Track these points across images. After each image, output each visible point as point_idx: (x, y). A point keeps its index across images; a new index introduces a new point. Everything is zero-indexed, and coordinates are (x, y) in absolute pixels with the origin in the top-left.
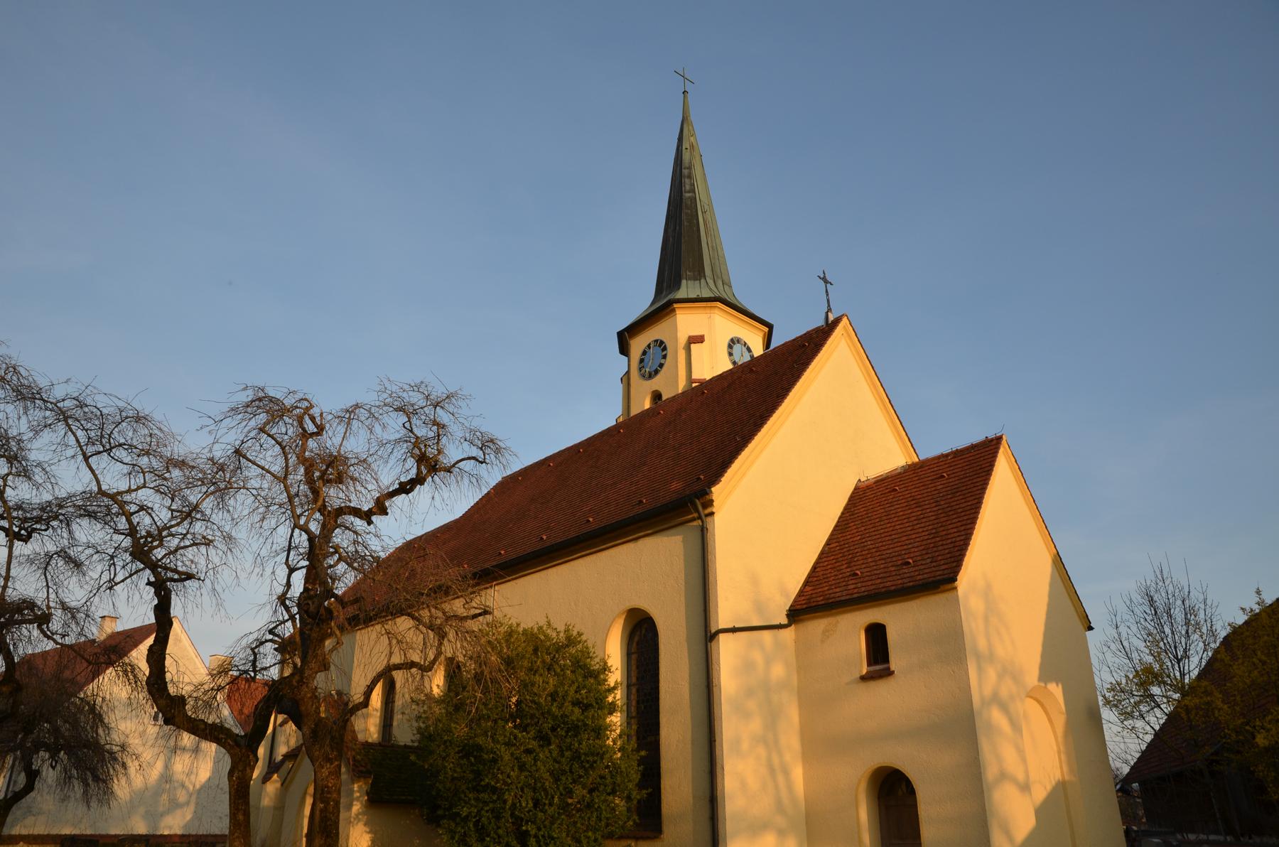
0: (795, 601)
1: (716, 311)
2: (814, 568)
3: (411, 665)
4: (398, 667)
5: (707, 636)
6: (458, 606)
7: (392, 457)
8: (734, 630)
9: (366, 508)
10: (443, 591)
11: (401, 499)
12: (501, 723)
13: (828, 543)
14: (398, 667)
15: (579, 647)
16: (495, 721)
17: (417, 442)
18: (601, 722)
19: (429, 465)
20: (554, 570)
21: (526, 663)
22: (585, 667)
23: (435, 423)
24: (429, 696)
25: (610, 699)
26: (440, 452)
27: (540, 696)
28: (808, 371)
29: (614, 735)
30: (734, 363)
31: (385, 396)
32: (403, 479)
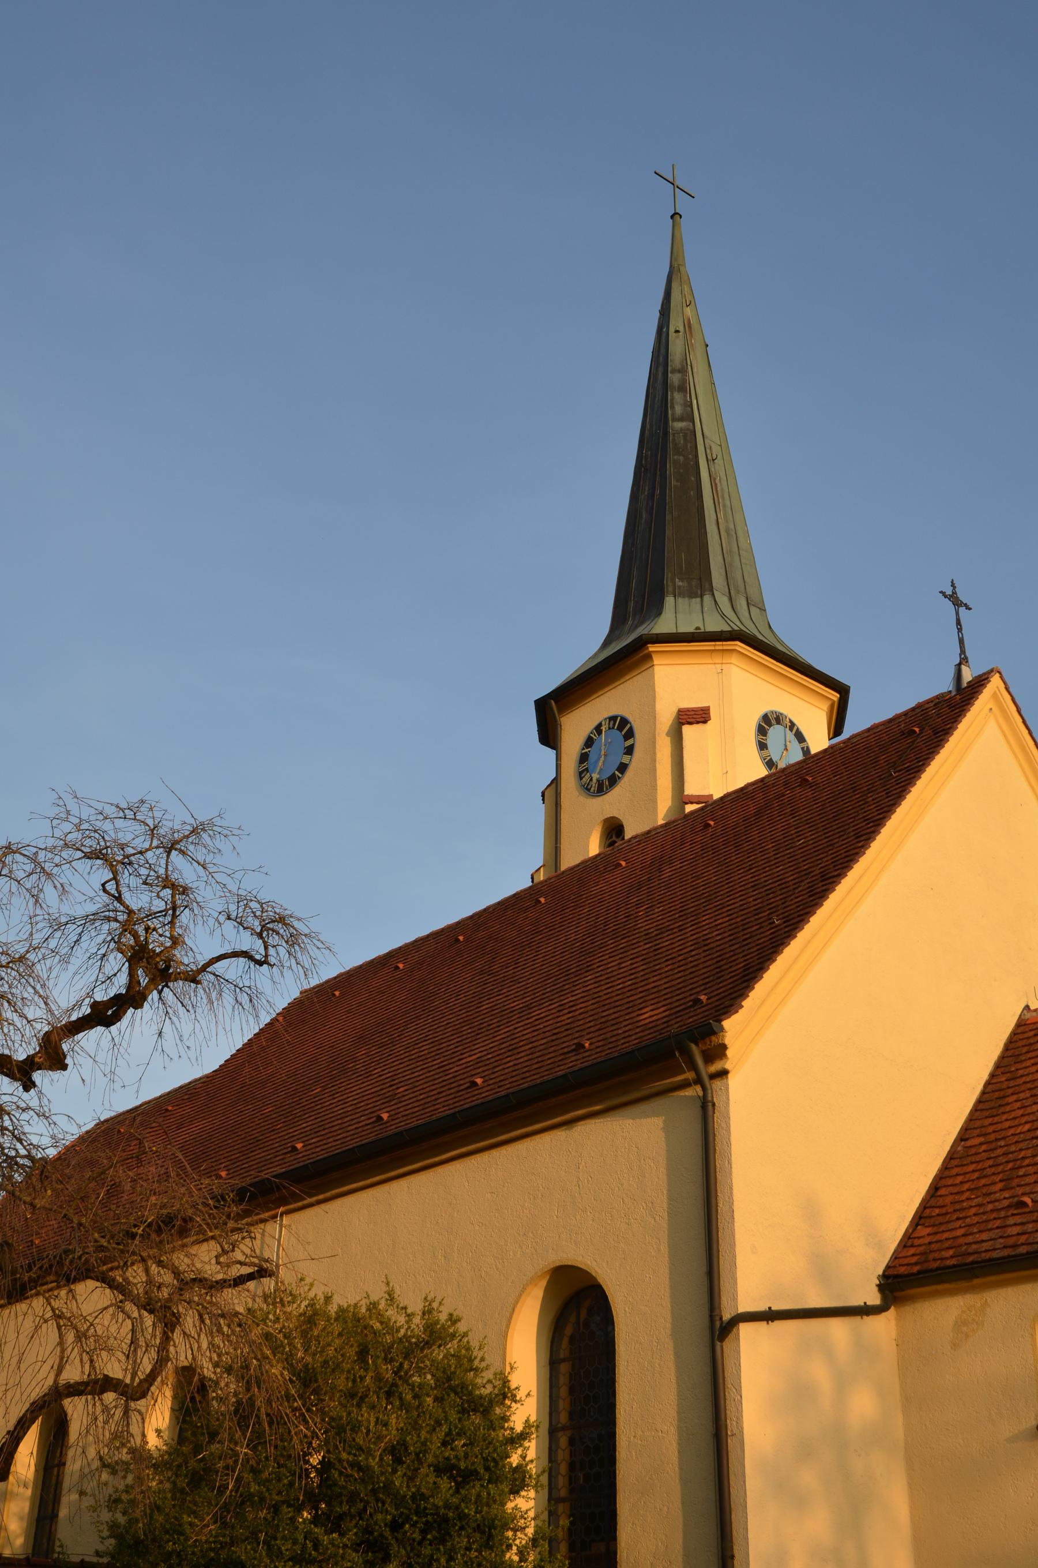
0: (895, 1256)
1: (734, 659)
2: (935, 1188)
3: (103, 1385)
4: (75, 1390)
5: (714, 1328)
6: (203, 1258)
7: (78, 951)
8: (769, 1316)
9: (21, 1056)
10: (175, 1227)
11: (93, 1038)
12: (286, 1511)
13: (962, 1137)
14: (75, 1390)
15: (452, 1346)
16: (276, 1509)
17: (131, 920)
18: (495, 1509)
19: (153, 968)
20: (403, 1183)
21: (342, 1382)
22: (463, 1390)
23: (167, 883)
24: (140, 1454)
25: (515, 1460)
26: (176, 941)
27: (369, 1453)
28: (920, 784)
29: (521, 1539)
30: (770, 764)
31: (67, 827)
32: (100, 996)
